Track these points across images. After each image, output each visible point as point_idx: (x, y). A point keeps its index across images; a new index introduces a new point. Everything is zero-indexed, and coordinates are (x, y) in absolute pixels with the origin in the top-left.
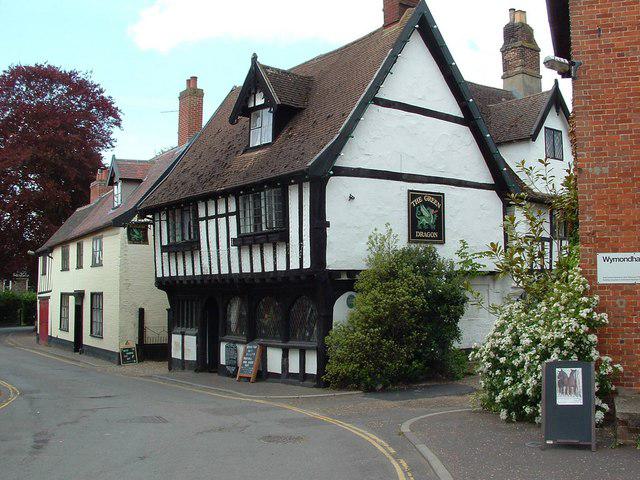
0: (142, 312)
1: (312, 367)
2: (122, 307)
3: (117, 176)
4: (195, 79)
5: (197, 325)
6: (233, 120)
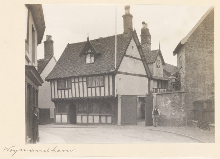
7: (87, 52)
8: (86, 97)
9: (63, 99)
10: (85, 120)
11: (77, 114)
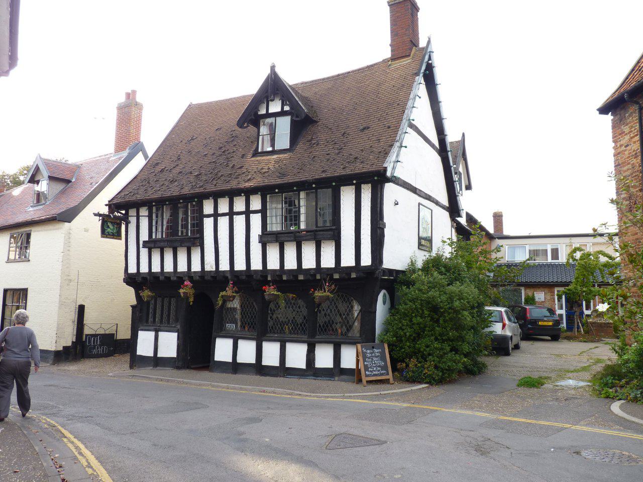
0: (81, 309)
1: (349, 359)
2: (62, 304)
3: (45, 173)
4: (134, 92)
5: (177, 320)
6: (241, 123)
7: (263, 111)
8: (256, 271)
9: (166, 277)
10: (247, 352)
11: (214, 334)
